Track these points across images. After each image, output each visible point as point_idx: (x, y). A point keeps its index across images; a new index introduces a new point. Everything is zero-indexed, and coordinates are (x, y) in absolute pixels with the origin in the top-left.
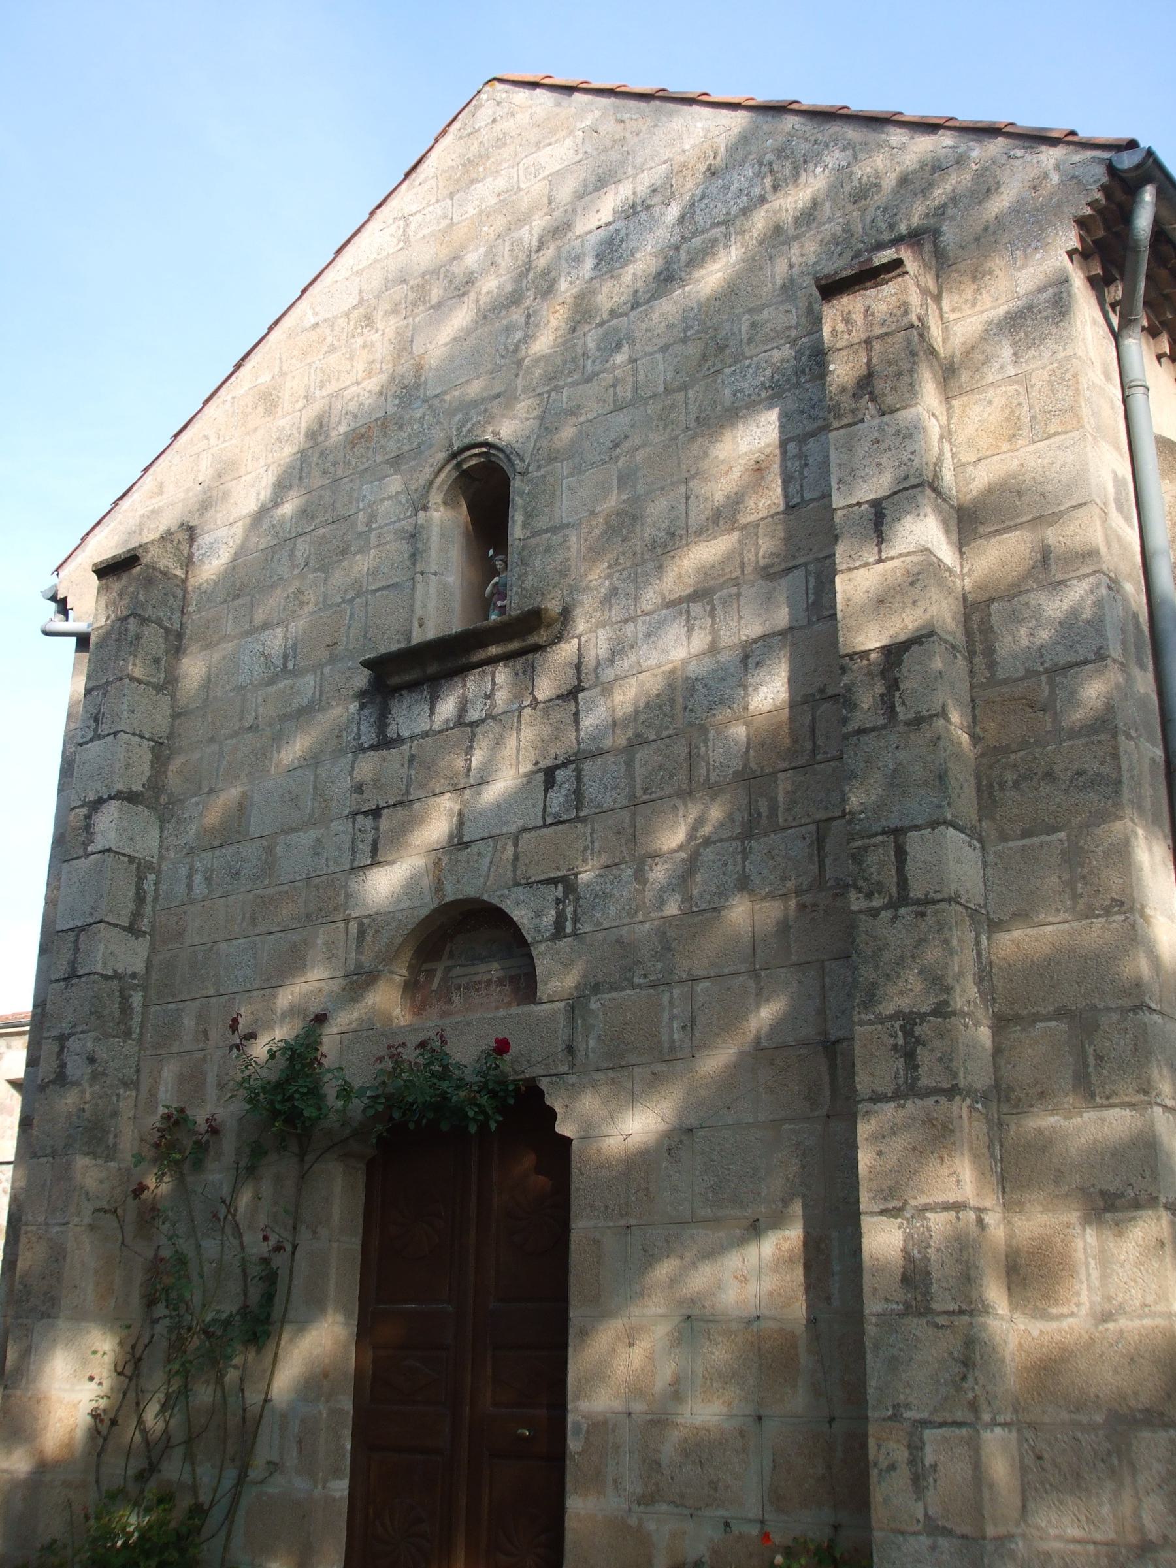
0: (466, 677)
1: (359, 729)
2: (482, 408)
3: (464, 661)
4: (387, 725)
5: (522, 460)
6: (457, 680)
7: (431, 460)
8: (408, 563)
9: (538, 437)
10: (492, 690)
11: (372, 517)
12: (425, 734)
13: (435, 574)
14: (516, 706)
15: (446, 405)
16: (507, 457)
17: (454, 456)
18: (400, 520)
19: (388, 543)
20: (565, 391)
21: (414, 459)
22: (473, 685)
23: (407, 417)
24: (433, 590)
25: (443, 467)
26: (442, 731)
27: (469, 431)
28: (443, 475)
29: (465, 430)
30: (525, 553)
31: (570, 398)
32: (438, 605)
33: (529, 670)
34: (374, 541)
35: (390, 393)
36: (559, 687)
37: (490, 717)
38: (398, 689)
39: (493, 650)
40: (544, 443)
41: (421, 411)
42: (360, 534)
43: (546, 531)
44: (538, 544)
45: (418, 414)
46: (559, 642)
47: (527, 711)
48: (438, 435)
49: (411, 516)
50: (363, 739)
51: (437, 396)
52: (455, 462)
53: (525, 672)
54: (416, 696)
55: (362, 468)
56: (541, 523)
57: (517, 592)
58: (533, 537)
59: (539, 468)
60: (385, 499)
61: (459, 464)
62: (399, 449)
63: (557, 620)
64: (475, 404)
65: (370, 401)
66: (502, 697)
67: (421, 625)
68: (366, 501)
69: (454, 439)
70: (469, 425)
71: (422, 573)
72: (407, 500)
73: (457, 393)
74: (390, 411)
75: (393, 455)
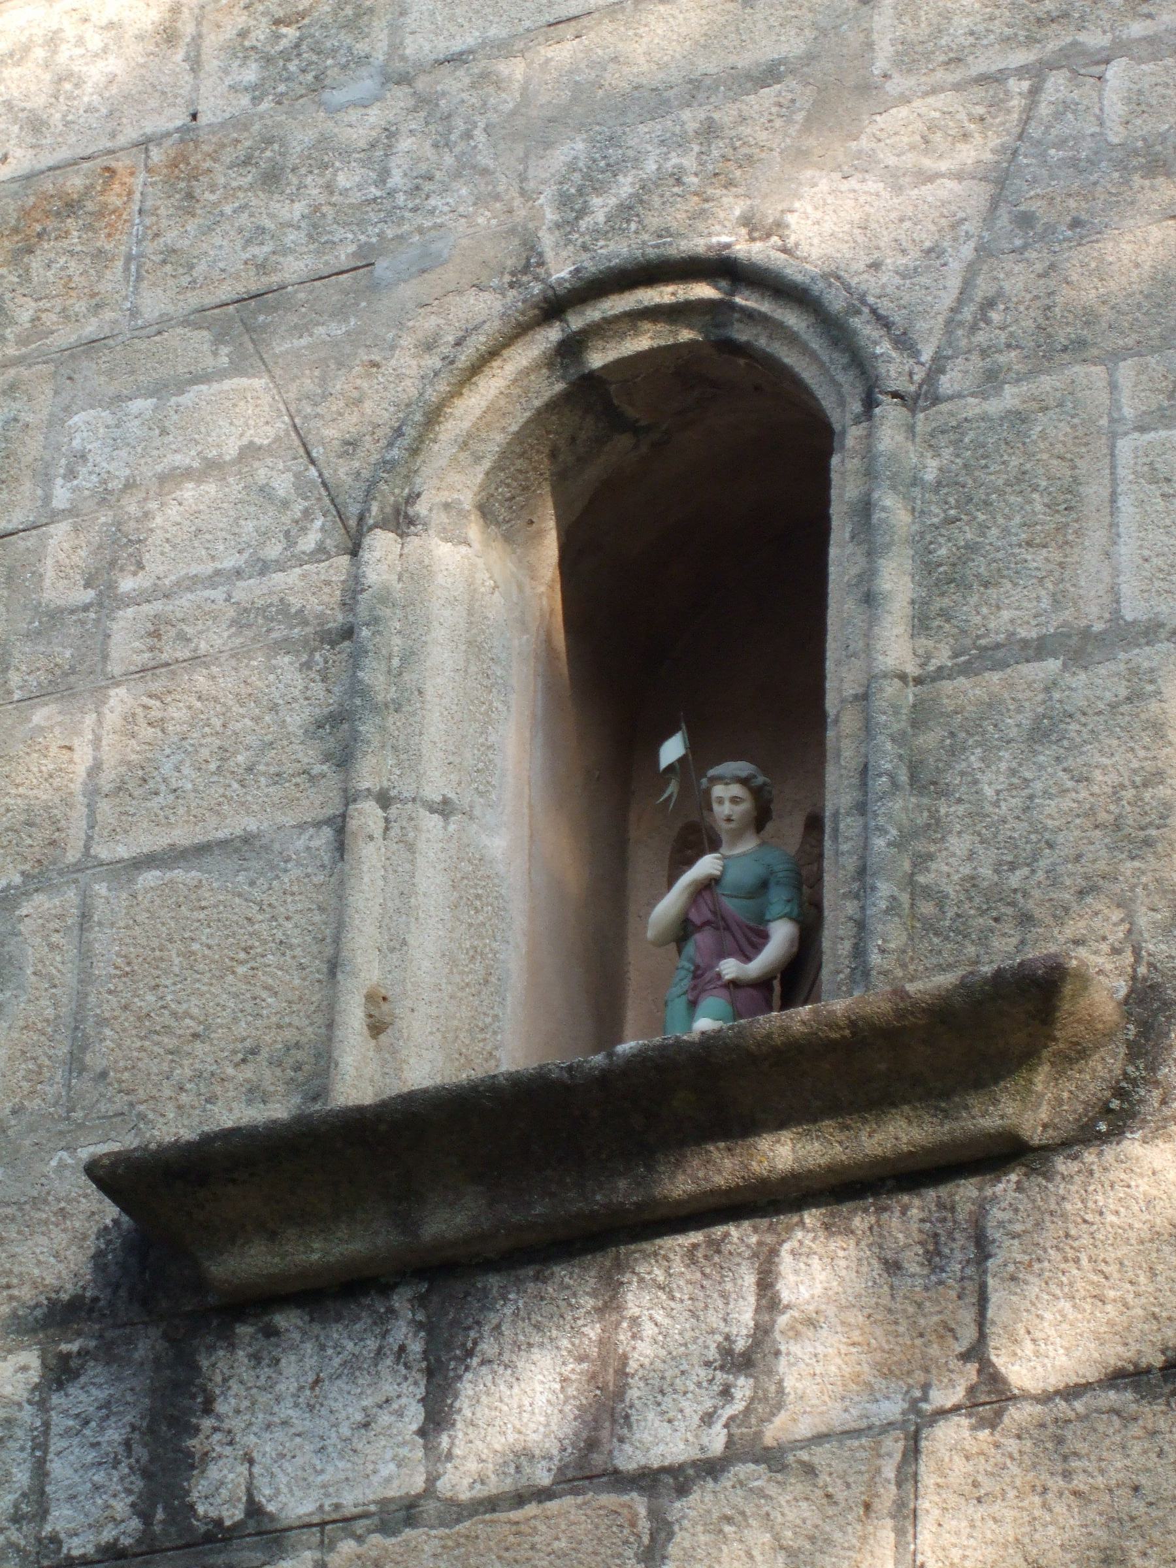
0: (620, 1266)
1: (40, 1471)
2: (691, 119)
3: (622, 1191)
4: (193, 1463)
5: (905, 343)
6: (576, 1283)
7: (429, 323)
8: (308, 755)
9: (984, 251)
10: (762, 1332)
11: (120, 549)
12: (402, 1514)
13: (444, 809)
14: (892, 1409)
15: (508, 101)
16: (835, 329)
17: (553, 308)
18: (264, 568)
19: (196, 660)
20: (1115, 72)
21: (340, 313)
22: (665, 1307)
23: (301, 138)
24: (431, 883)
25: (493, 353)
26: (491, 1504)
27: (626, 211)
28: (493, 385)
29: (601, 207)
30: (929, 739)
31: (1137, 102)
32: (446, 954)
33: (959, 1250)
34: (125, 642)
35: (213, 40)
36: (1123, 1335)
37: (753, 1451)
38: (253, 1307)
39: (781, 1153)
40: (1016, 278)
41: (375, 115)
42: (55, 617)
43: (1039, 649)
44: (992, 704)
45: (358, 129)
46: (1117, 1133)
47: (951, 1438)
48: (468, 223)
49: (321, 553)
50: (61, 1518)
51: (456, 59)
52: (553, 334)
53: (934, 1256)
54: (348, 1339)
55: (66, 336)
56: (1012, 612)
57: (893, 907)
58: (966, 670)
59: (992, 379)
60: (187, 474)
61: (570, 349)
62: (262, 267)
63: (1109, 1035)
64: (654, 101)
65: (113, 64)
66: (819, 1376)
67: (377, 1028)
68: (86, 480)
69: (547, 241)
70: (625, 186)
71: (384, 800)
72: (301, 486)
73: (562, 53)
74: (215, 106)
75: (225, 292)
